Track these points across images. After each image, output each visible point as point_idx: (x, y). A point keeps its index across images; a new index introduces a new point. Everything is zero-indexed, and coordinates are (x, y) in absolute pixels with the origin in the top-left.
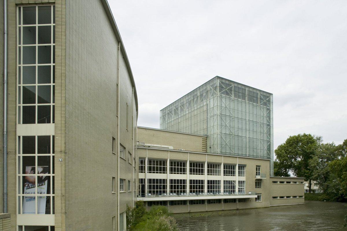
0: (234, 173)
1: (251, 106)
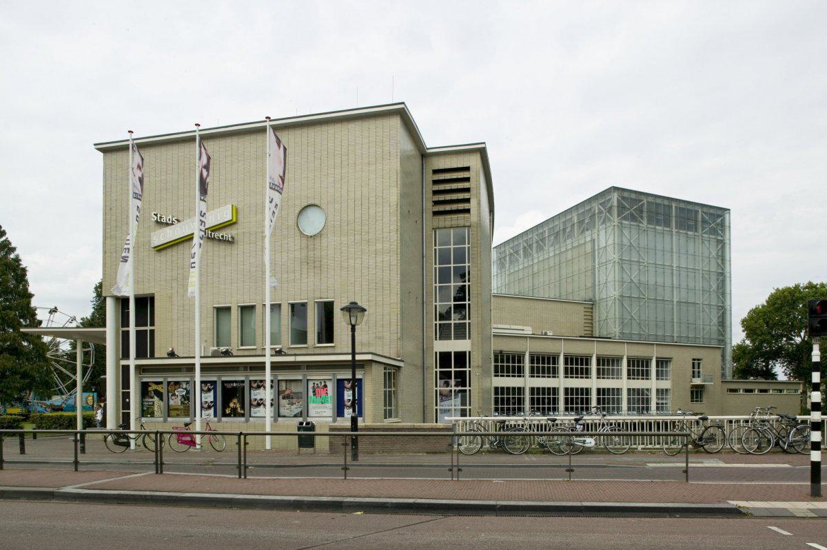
0: (647, 375)
1: (683, 239)
